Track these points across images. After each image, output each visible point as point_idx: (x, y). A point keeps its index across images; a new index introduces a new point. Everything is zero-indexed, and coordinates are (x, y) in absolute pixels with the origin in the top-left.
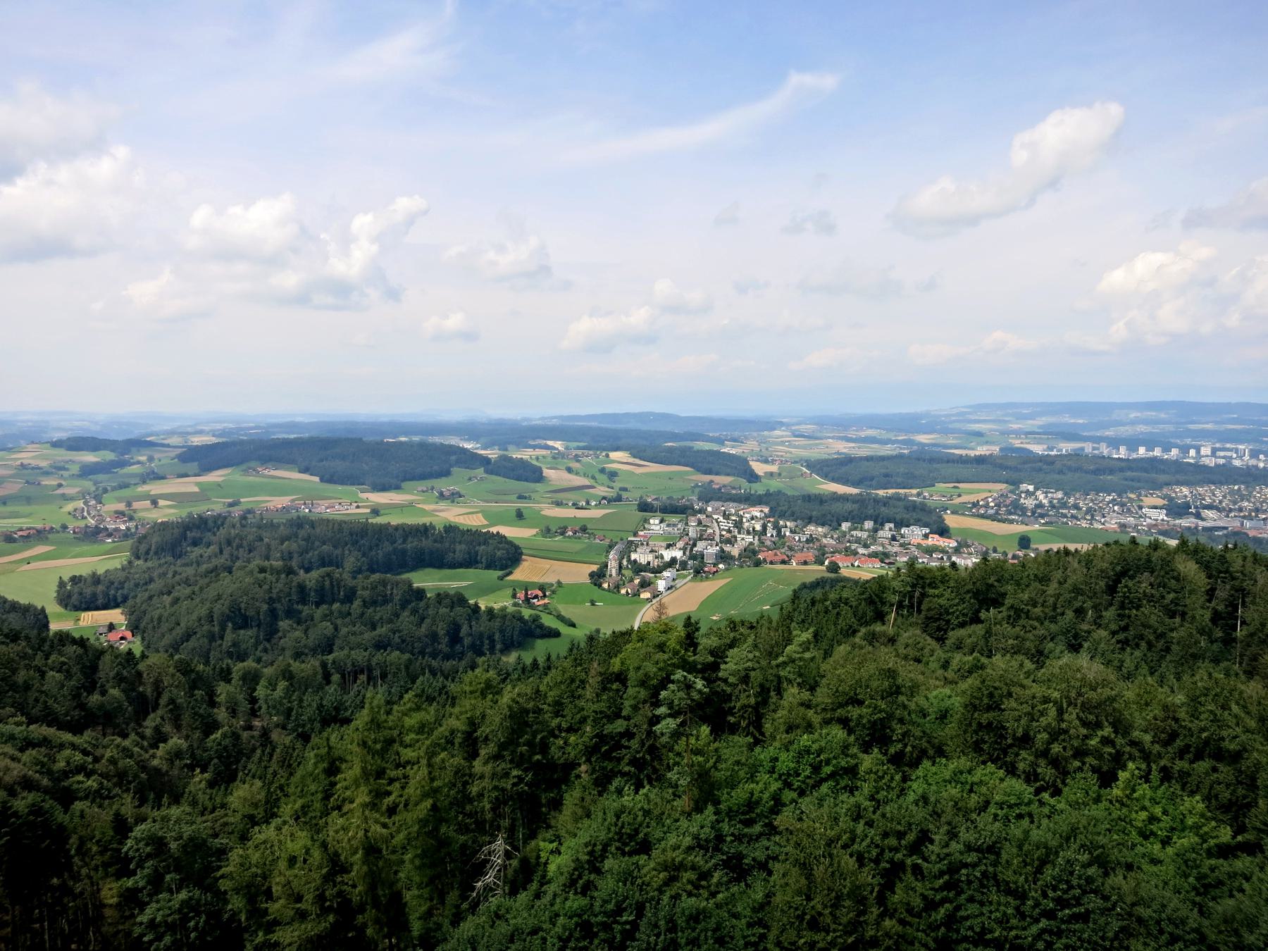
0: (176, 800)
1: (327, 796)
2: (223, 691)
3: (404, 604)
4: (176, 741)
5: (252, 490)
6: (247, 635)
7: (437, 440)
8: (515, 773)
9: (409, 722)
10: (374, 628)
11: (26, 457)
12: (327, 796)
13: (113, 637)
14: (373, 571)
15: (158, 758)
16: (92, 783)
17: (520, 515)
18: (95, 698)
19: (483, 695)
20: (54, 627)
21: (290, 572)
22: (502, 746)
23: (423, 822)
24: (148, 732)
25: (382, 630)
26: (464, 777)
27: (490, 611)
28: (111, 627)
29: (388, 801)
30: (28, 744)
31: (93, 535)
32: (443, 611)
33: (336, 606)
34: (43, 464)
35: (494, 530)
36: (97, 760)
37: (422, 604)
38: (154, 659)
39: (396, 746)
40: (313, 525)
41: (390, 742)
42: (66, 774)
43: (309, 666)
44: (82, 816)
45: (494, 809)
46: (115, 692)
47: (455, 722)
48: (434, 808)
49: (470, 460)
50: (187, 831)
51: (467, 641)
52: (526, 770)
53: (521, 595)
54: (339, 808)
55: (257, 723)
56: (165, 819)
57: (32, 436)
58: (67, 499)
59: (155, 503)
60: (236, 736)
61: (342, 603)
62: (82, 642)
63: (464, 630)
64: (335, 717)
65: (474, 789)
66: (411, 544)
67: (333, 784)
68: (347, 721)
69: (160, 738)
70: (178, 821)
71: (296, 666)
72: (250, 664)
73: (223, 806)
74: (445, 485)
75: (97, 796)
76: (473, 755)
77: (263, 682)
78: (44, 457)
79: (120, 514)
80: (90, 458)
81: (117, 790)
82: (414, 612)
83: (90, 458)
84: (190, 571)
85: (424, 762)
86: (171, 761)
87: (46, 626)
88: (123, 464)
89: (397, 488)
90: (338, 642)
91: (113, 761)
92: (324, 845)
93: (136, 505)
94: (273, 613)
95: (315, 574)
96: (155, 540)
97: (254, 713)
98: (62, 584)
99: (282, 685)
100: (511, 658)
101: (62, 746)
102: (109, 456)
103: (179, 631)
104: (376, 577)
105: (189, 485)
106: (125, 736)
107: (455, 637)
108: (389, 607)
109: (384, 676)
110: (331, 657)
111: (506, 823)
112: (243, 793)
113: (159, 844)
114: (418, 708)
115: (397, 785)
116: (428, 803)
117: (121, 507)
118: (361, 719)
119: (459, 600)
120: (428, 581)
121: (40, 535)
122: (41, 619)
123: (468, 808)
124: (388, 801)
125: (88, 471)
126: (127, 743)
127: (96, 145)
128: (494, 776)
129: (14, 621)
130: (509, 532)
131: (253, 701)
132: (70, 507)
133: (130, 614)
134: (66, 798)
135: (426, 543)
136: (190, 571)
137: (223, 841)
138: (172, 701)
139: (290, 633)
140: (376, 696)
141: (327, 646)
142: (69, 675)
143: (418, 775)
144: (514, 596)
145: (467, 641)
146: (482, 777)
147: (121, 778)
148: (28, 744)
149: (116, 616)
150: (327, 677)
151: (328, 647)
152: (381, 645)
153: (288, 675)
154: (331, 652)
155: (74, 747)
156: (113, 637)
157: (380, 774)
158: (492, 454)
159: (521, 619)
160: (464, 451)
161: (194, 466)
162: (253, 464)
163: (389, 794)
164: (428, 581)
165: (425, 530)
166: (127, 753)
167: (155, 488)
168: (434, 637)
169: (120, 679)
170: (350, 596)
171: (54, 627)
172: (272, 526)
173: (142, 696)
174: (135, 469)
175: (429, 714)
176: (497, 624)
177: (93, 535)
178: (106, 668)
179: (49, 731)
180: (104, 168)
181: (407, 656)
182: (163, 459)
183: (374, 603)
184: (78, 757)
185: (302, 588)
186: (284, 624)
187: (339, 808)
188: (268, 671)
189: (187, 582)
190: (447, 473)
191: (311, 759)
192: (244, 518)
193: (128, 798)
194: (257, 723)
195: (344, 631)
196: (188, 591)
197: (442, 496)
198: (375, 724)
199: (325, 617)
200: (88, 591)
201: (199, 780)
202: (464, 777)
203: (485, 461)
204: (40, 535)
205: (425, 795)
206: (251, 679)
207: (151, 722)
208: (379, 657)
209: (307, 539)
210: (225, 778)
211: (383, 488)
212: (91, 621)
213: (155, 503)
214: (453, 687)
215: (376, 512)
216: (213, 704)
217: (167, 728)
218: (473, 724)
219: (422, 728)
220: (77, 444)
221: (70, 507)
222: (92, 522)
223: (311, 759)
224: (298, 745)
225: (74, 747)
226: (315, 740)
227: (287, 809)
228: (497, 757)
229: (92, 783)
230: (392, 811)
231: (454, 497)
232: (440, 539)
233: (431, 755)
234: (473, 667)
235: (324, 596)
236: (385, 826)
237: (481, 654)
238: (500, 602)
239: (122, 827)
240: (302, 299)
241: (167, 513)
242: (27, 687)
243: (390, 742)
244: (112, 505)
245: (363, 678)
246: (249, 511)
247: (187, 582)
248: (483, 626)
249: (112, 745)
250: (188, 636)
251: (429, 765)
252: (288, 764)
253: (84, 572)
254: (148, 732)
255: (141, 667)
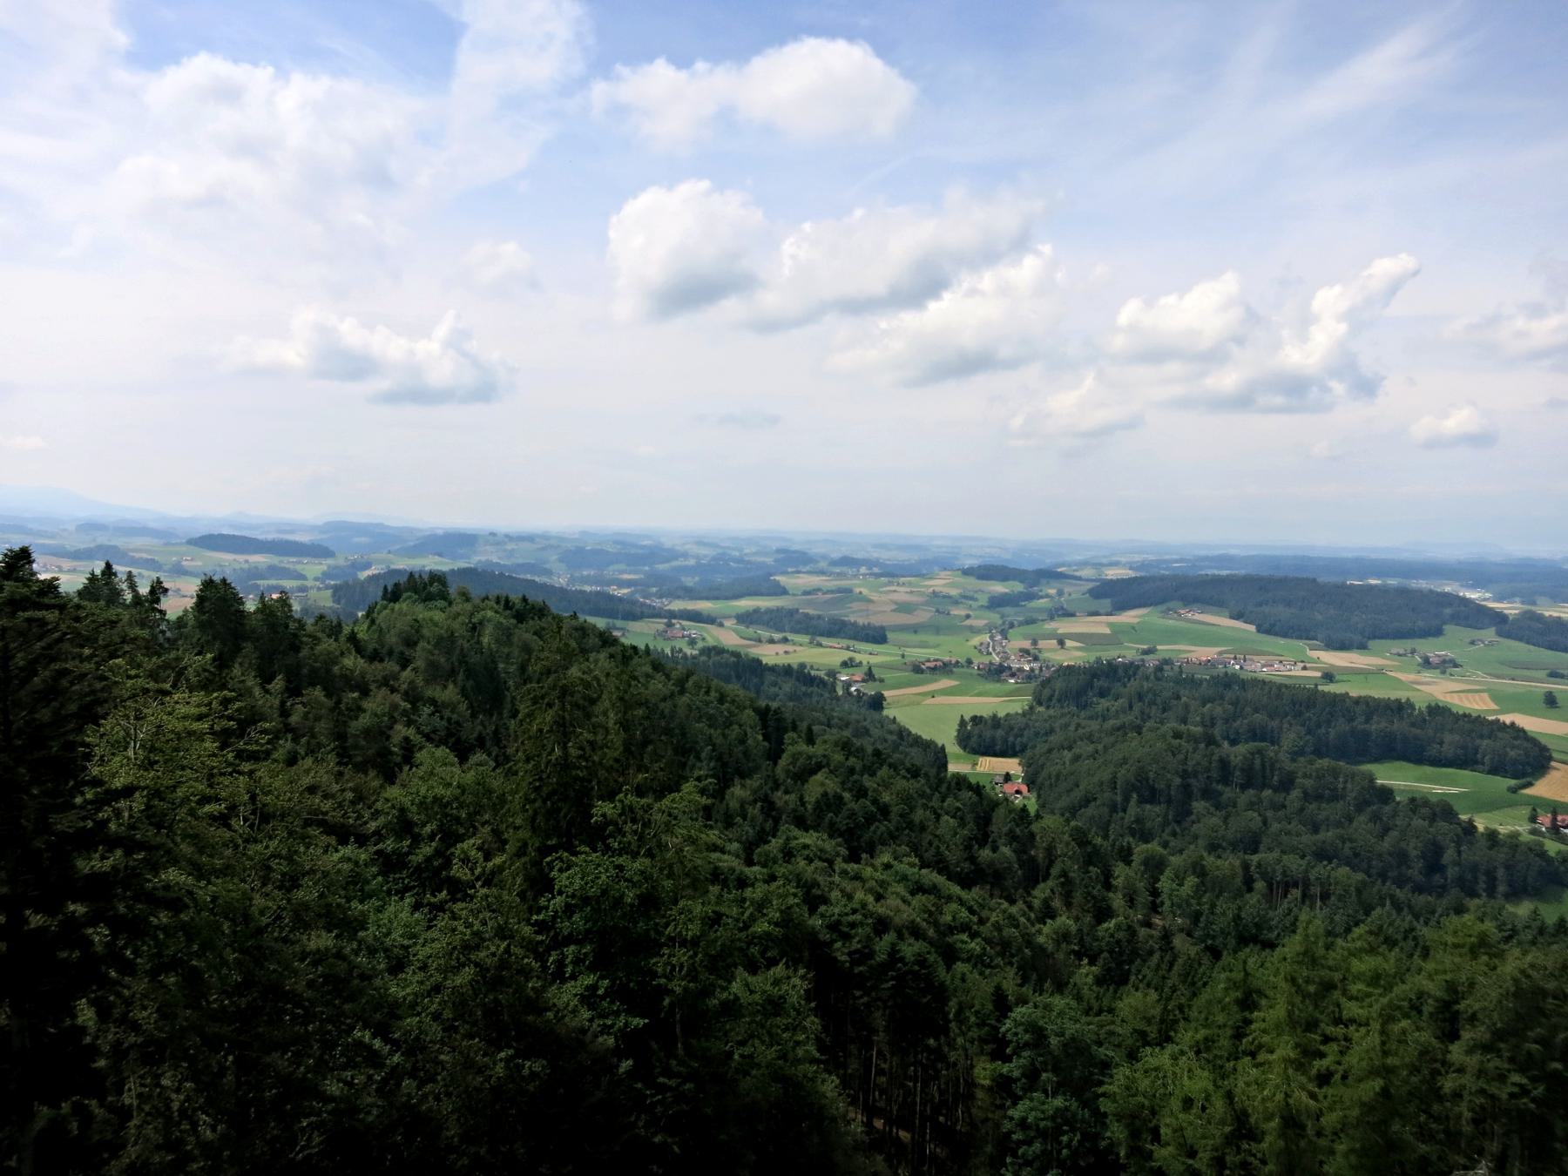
0: (1060, 987)
1: (1238, 1035)
2: (1122, 874)
3: (1361, 805)
4: (1064, 921)
5: (1172, 636)
6: (1154, 811)
7: (1423, 584)
8: (1516, 1078)
9: (1358, 966)
10: (1316, 829)
11: (941, 583)
12: (1238, 1035)
13: (1009, 788)
14: (1318, 753)
15: (1045, 934)
16: (975, 946)
17: (1551, 701)
18: (985, 854)
19: (1474, 952)
20: (953, 768)
21: (1210, 741)
22: (1499, 1035)
23: (1368, 1108)
24: (1037, 903)
25: (1327, 835)
26: (1432, 1065)
27: (1492, 835)
28: (1008, 778)
29: (1319, 1065)
30: (919, 889)
31: (997, 673)
32: (1418, 822)
33: (1268, 793)
34: (954, 592)
35: (1507, 719)
36: (982, 922)
37: (1387, 809)
38: (1050, 821)
39: (1336, 994)
40: (1244, 684)
41: (1328, 987)
42: (951, 930)
43: (1227, 864)
44: (963, 980)
45: (1476, 1122)
46: (1006, 851)
47: (1427, 981)
48: (1385, 1093)
49: (1475, 616)
50: (1071, 1029)
51: (1452, 872)
52: (1534, 1080)
53: (1545, 820)
54: (1253, 1055)
55: (1157, 921)
56: (1048, 1007)
57: (945, 565)
58: (975, 631)
59: (1061, 643)
60: (1131, 931)
61: (1276, 790)
62: (977, 789)
63: (1449, 855)
64: (1254, 937)
65: (1448, 1084)
66: (1377, 726)
67: (1248, 1022)
68: (1271, 945)
69: (1048, 913)
70: (1061, 1014)
71: (1210, 860)
72: (1154, 847)
73: (1111, 1011)
74: (1435, 649)
75: (978, 961)
76: (1453, 1036)
77: (1168, 872)
78: (952, 585)
79: (1025, 652)
80: (999, 588)
81: (999, 960)
82: (1375, 818)
83: (999, 588)
84: (1094, 726)
85: (1376, 1026)
86: (1058, 943)
87: (945, 766)
88: (1031, 597)
89: (1362, 647)
90: (1265, 841)
91: (998, 927)
92: (1229, 1096)
93: (1042, 644)
94: (1186, 789)
95: (1242, 749)
96: (1059, 685)
97: (1155, 908)
98: (963, 723)
99: (1191, 881)
100: (1522, 910)
101: (949, 898)
102: (1017, 587)
103: (1077, 794)
104: (1324, 763)
105: (1099, 626)
106: (1012, 902)
107: (1434, 864)
108: (1340, 805)
109: (1325, 897)
110: (1255, 858)
111: (1494, 1147)
112: (1135, 1002)
113: (1038, 1036)
114: (1372, 950)
115: (1334, 1047)
116: (1377, 1084)
117: (1027, 644)
118: (1292, 946)
119: (1444, 811)
120: (1398, 778)
121: (944, 669)
122: (940, 757)
123: (1436, 1108)
124: (1319, 1065)
125: (996, 603)
126: (1014, 910)
127: (1021, 244)
128: (1481, 1073)
129: (916, 757)
130: (1532, 724)
131: (1155, 893)
132: (976, 640)
133: (1027, 765)
134: (950, 955)
135: (1399, 727)
136: (1094, 726)
137: (1104, 1052)
138: (1064, 874)
139: (1205, 817)
140: (1314, 920)
141: (1252, 843)
142: (963, 823)
143: (1366, 1042)
144: (1533, 819)
145: (1452, 872)
146: (1461, 1070)
147: (1005, 946)
148: (919, 889)
149: (1013, 766)
150: (1249, 884)
151: (1252, 843)
152: (1323, 854)
153: (1199, 870)
154: (1255, 851)
155: (961, 902)
156: (1009, 788)
157: (1311, 1026)
158: (1511, 609)
159: (1542, 854)
160: (1466, 602)
161: (1106, 603)
162: (1171, 604)
163: (1322, 1055)
164: (1398, 778)
165: (1399, 708)
166: (1011, 917)
167: (1063, 627)
168: (1402, 857)
169: (1012, 837)
170: (1287, 784)
171: (953, 768)
172: (1192, 682)
173: (1033, 859)
174: (1042, 603)
175: (1387, 962)
176: (1501, 855)
177: (997, 673)
178: (1000, 823)
179: (940, 880)
180: (1027, 270)
181: (1360, 876)
182: (1074, 593)
183: (1319, 798)
184: (964, 914)
185: (1224, 764)
186: (1199, 806)
187: (1253, 1055)
188: (1175, 860)
189: (1090, 738)
190: (1438, 632)
191: (1220, 984)
192: (1159, 669)
193: (1011, 972)
194: (1157, 921)
195: (1275, 827)
196: (1091, 748)
197: (1427, 663)
198: (1309, 958)
199: (1251, 806)
200: (988, 734)
201: (1085, 974)
202: (1432, 1065)
203: (1499, 619)
204: (944, 669)
205: (1373, 1073)
206: (1155, 867)
207: (1041, 892)
208: (1320, 870)
209: (1235, 703)
210: (1114, 978)
211: (1343, 646)
212: (989, 766)
213: (1061, 643)
214: (1425, 932)
215: (1329, 677)
216: (1108, 886)
217: (1057, 903)
218: (1454, 992)
219: (1375, 979)
220: (987, 572)
221: (976, 640)
222: (996, 659)
223: (1220, 984)
224: (1206, 960)
225: (961, 902)
226: (1226, 958)
227: (1187, 1036)
228: (1486, 1048)
229: (975, 946)
230: (1324, 1079)
231: (1446, 666)
232: (1420, 722)
233: (1387, 1019)
234: (1460, 910)
235: (1253, 778)
236: (1313, 1096)
237: (1473, 894)
238: (1510, 824)
239: (1002, 1005)
240: (1242, 401)
241: (1074, 656)
242: (923, 828)
243: (1328, 987)
244: (1018, 642)
245: (1296, 893)
246: (1167, 662)
247: (1090, 738)
248: (1476, 854)
249: (999, 911)
250: (1087, 801)
251: (1383, 1032)
252: (1193, 981)
253: (985, 713)
254: (1037, 903)
255: (1035, 827)
